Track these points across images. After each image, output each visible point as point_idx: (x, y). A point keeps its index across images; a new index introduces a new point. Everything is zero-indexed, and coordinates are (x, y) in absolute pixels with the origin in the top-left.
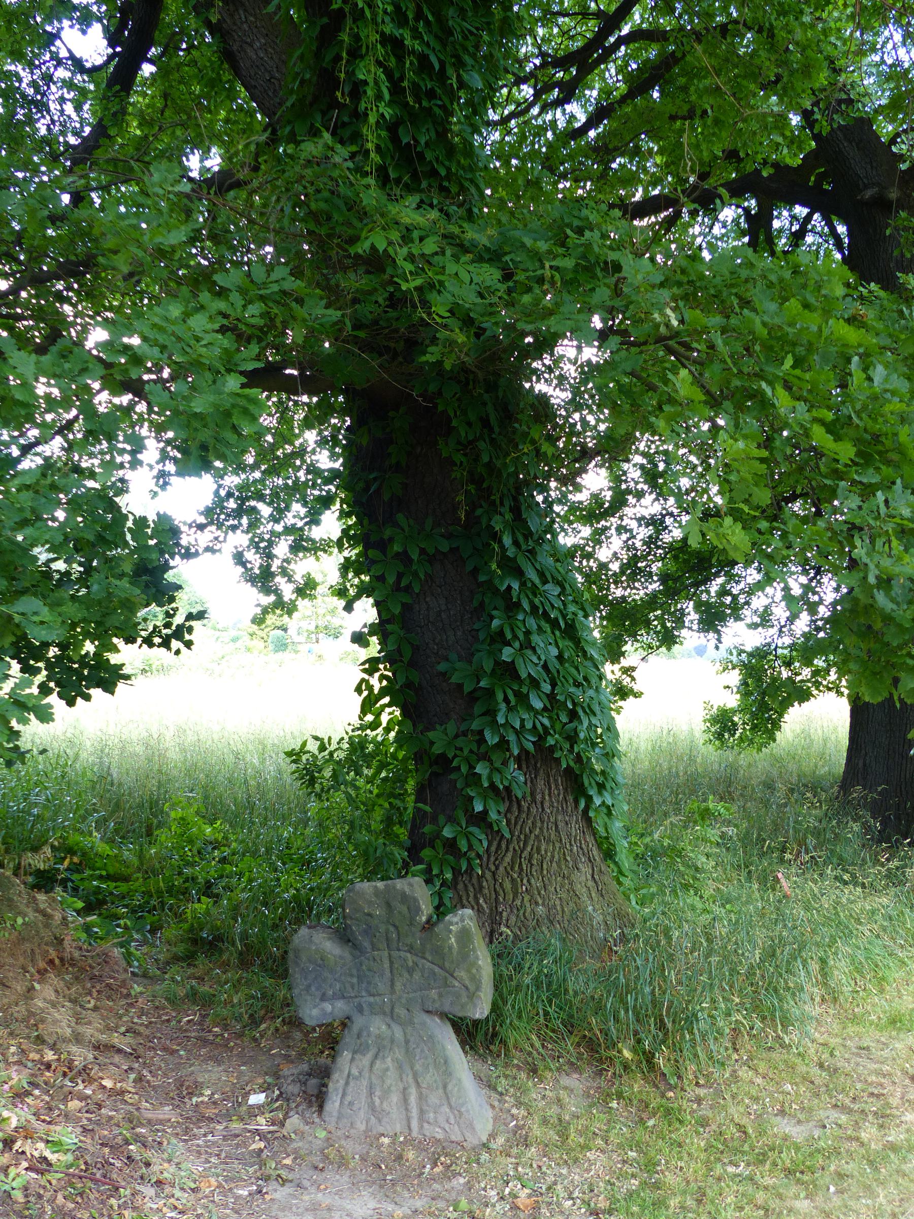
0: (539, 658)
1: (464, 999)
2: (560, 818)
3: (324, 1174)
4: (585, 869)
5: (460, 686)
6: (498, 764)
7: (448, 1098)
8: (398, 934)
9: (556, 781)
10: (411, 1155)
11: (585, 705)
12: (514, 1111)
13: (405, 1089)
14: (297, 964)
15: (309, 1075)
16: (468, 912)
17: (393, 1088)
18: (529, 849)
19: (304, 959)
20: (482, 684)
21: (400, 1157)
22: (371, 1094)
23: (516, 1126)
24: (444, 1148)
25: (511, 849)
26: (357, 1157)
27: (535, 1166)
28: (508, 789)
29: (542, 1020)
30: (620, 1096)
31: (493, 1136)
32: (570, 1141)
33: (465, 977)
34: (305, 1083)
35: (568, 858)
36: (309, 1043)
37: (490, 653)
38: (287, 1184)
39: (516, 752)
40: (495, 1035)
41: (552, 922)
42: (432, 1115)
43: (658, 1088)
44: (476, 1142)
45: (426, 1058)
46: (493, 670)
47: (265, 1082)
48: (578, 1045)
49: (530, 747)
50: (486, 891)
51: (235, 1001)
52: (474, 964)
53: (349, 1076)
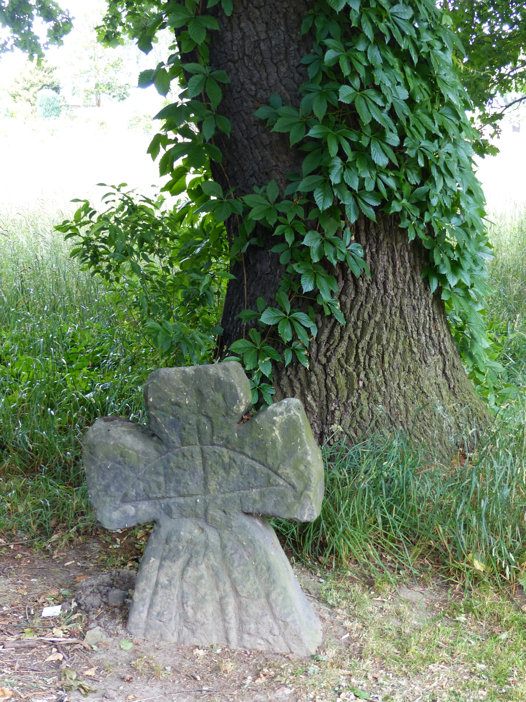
0: (385, 100)
1: (290, 500)
2: (405, 301)
3: (132, 685)
4: (434, 359)
5: (284, 137)
6: (330, 235)
7: (271, 607)
8: (212, 427)
9: (402, 257)
10: (229, 666)
11: (441, 164)
12: (347, 623)
13: (221, 598)
14: (93, 462)
15: (111, 586)
16: (296, 401)
17: (208, 598)
18: (367, 338)
19: (101, 455)
20: (312, 133)
21: (217, 669)
22: (183, 603)
23: (349, 639)
24: (267, 660)
25: (346, 338)
26: (168, 668)
27: (370, 677)
28: (342, 265)
29: (380, 528)
30: (468, 609)
31: (322, 648)
32: (410, 653)
33: (291, 475)
34: (106, 595)
35: (415, 350)
36: (108, 554)
37: (323, 94)
38: (91, 695)
39: (353, 219)
40: (324, 545)
41: (393, 423)
42: (253, 626)
43: (513, 601)
44: (303, 654)
45: (246, 565)
46: (326, 117)
47: (60, 594)
48: (422, 556)
49: (371, 214)
50: (315, 387)
51: (21, 510)
52: (302, 460)
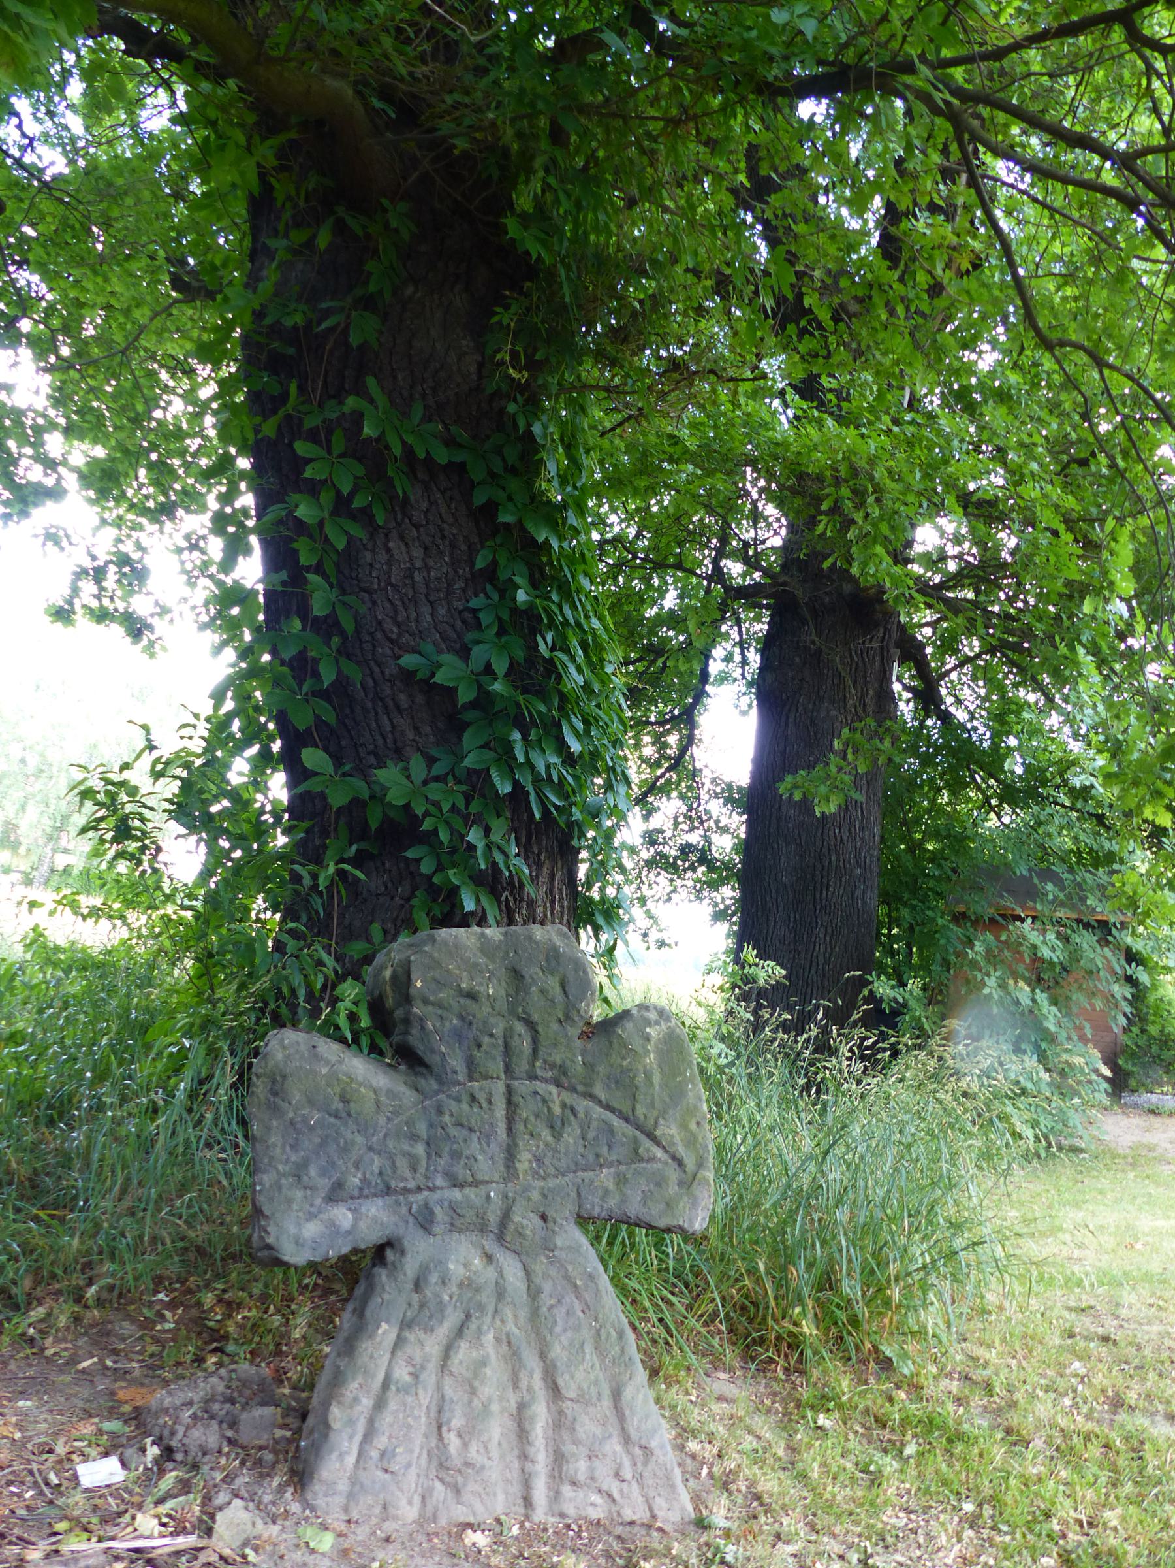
1: (673, 1189)
8: (535, 1042)
13: (522, 1407)
14: (275, 1109)
17: (495, 1407)
19: (296, 1097)
45: (577, 1328)
53: (385, 1385)
